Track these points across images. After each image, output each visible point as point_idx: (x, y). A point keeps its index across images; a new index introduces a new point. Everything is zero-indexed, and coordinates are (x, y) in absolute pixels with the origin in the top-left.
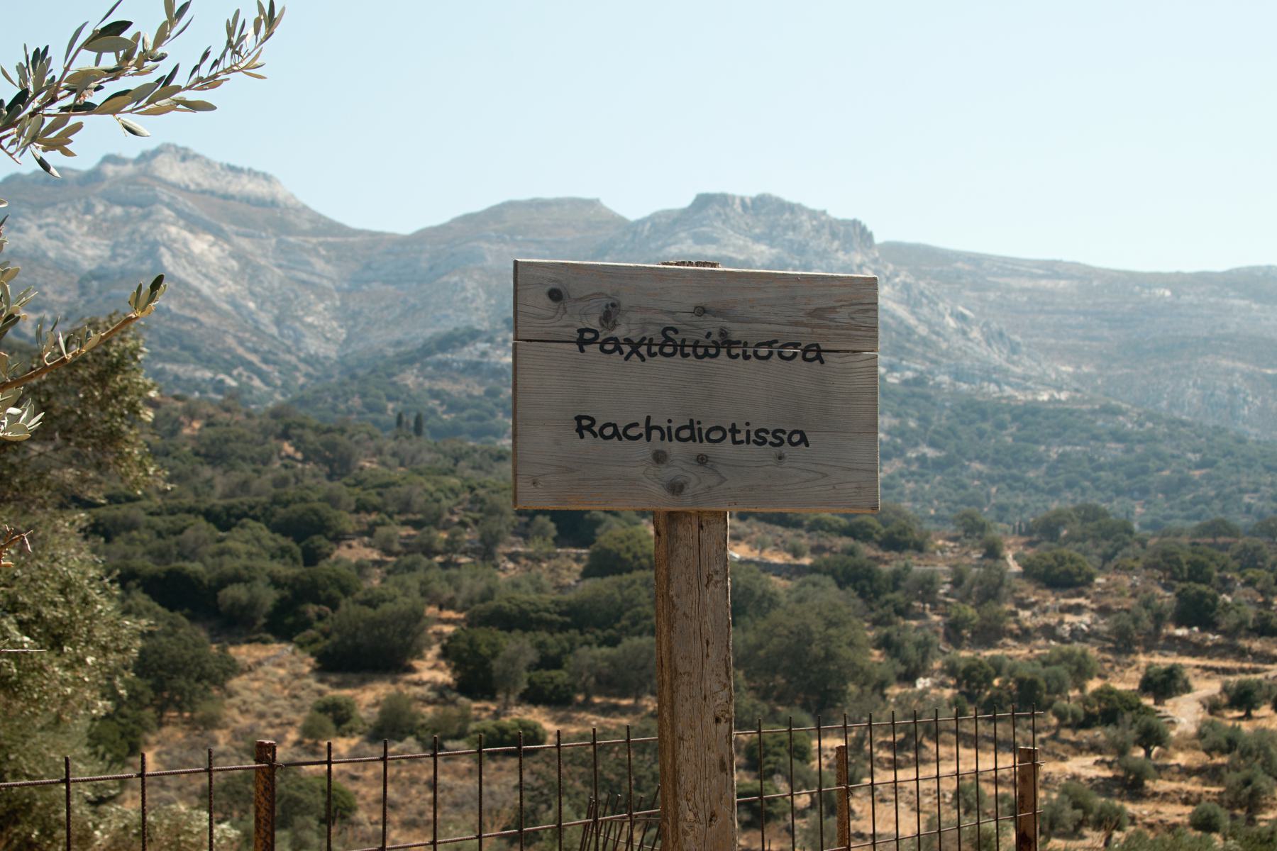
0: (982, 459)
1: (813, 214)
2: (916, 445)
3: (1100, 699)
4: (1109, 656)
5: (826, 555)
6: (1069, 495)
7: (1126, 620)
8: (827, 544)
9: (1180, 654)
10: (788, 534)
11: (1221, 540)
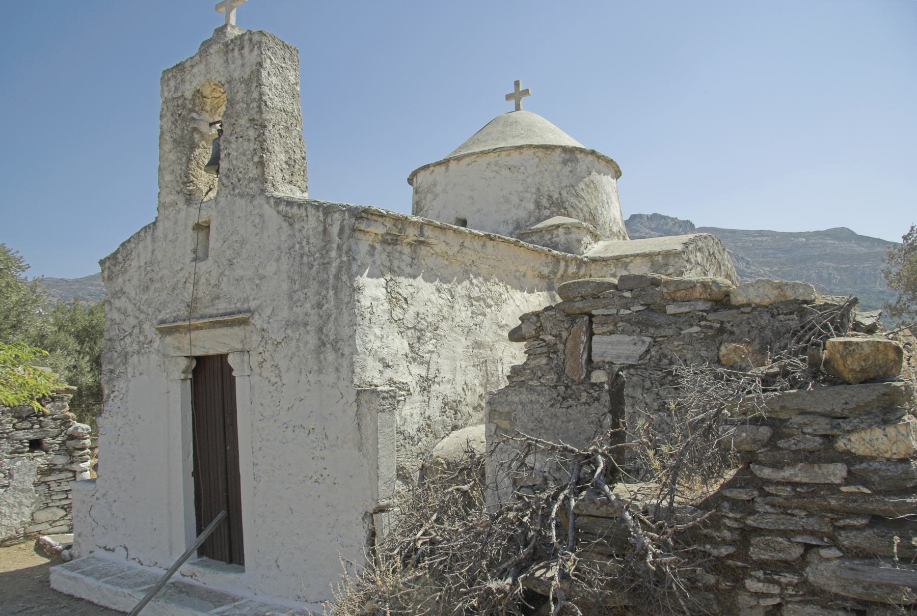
1: (673, 219)
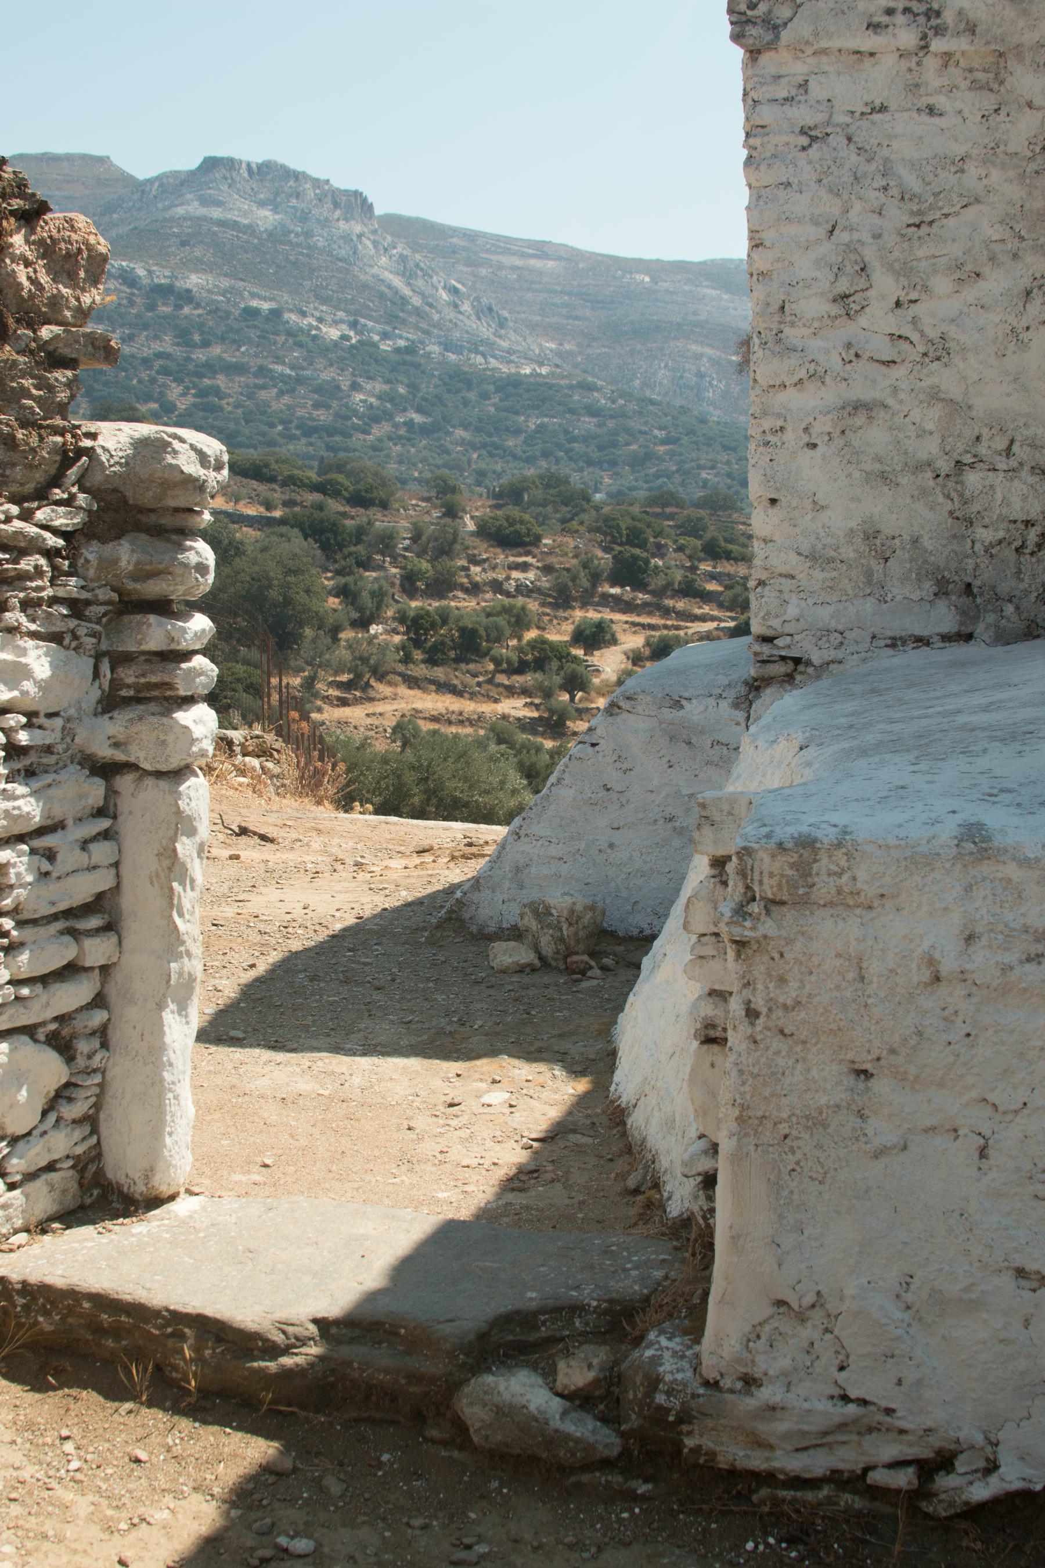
0: (466, 428)
1: (317, 183)
2: (405, 410)
3: (533, 648)
4: (548, 611)
5: (297, 509)
6: (544, 464)
7: (565, 578)
8: (298, 498)
9: (612, 611)
10: (262, 488)
11: (668, 510)
